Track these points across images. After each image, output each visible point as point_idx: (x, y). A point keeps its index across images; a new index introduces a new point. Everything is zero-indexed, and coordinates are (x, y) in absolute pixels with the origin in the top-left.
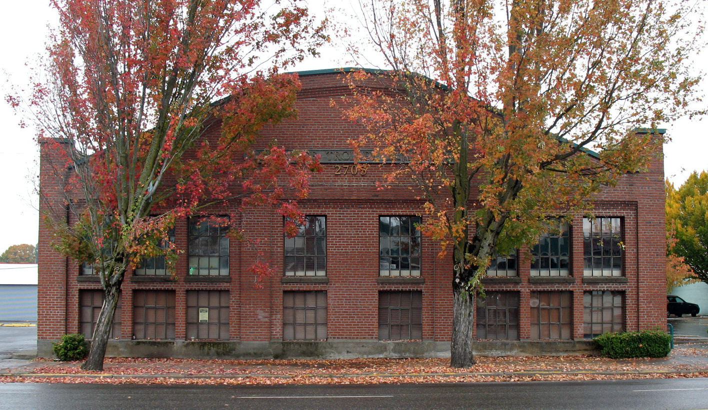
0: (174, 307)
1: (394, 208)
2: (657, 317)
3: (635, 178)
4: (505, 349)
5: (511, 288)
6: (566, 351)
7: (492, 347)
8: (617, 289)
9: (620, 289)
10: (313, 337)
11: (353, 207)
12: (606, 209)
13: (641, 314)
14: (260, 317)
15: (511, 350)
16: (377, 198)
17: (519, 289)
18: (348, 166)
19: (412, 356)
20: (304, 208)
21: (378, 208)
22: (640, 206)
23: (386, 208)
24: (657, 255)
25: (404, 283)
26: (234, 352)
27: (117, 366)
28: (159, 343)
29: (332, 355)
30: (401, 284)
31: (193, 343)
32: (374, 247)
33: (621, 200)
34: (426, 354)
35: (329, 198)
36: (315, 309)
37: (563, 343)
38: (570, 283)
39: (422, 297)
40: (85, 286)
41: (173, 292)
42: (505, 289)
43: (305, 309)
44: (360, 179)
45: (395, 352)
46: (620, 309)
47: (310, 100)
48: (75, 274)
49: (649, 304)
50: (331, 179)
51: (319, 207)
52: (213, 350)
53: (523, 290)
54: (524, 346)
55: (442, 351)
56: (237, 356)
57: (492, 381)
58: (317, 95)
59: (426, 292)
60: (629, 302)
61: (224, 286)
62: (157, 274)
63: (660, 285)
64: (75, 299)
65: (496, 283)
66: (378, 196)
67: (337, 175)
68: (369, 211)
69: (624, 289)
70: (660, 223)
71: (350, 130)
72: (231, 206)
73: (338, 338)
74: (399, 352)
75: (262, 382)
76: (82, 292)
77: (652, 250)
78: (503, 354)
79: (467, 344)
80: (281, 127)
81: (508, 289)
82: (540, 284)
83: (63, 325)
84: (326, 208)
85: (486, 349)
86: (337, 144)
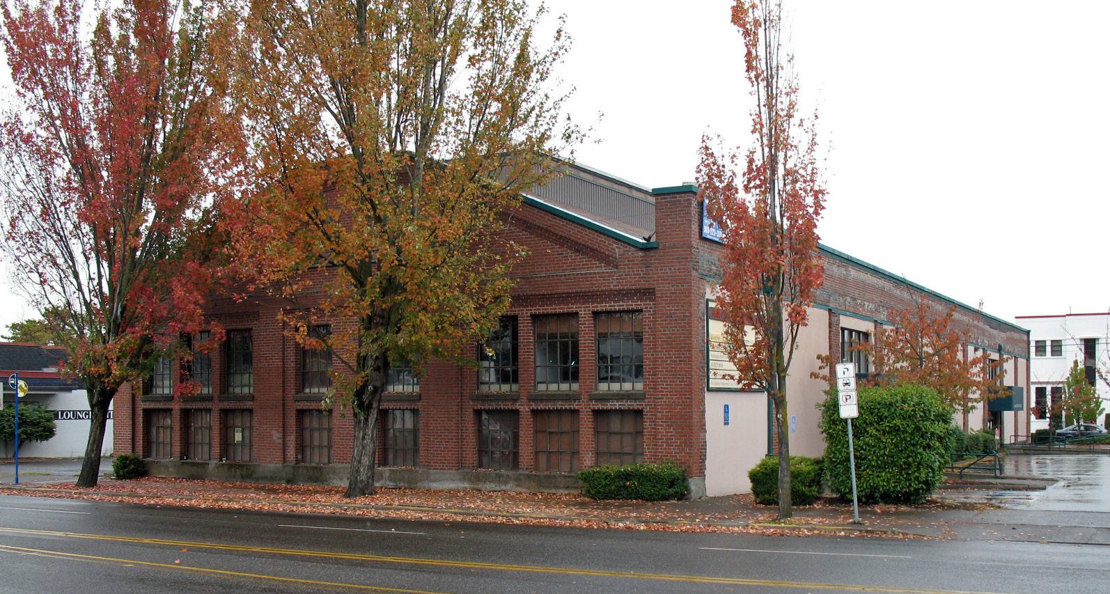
0: (578, 431)
2: (680, 446)
3: (653, 256)
4: (500, 482)
5: (510, 406)
6: (568, 487)
7: (486, 478)
8: (631, 408)
9: (636, 408)
10: (248, 458)
12: (619, 301)
14: (275, 438)
15: (506, 483)
17: (518, 407)
19: (406, 485)
24: (680, 361)
25: (402, 401)
26: (254, 476)
28: (198, 463)
29: (334, 481)
30: (399, 401)
31: (223, 464)
33: (634, 287)
34: (420, 484)
37: (564, 476)
38: (575, 400)
39: (643, 418)
40: (226, 405)
41: (575, 412)
42: (502, 407)
45: (390, 481)
48: (291, 391)
49: (670, 429)
52: (239, 472)
53: (522, 409)
54: (521, 480)
55: (434, 481)
56: (257, 480)
57: (331, 513)
61: (248, 405)
62: (572, 389)
63: (683, 402)
64: (140, 419)
65: (491, 401)
69: (640, 407)
70: (676, 320)
73: (343, 463)
74: (395, 481)
75: (266, 508)
76: (148, 413)
77: (674, 354)
78: (498, 488)
79: (360, 472)
81: (506, 408)
82: (541, 400)
85: (479, 481)
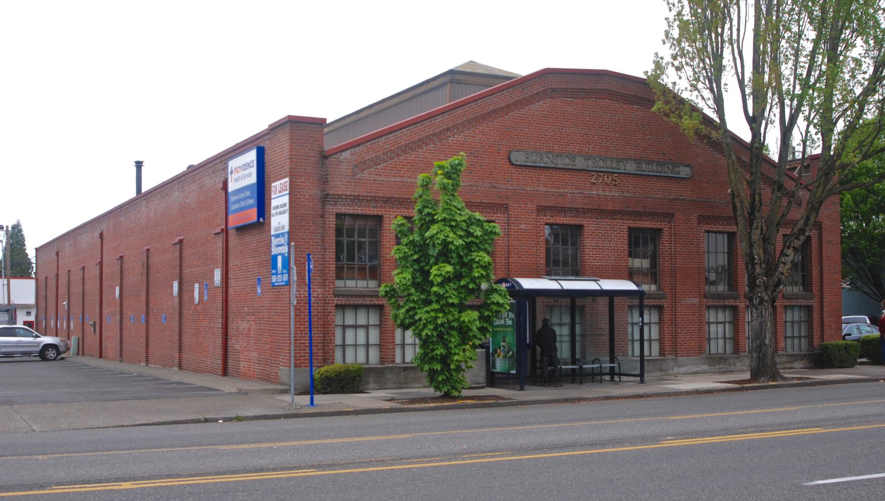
1: (640, 220)
11: (607, 217)
13: (825, 328)
16: (629, 209)
17: (738, 304)
18: (602, 174)
20: (565, 216)
21: (628, 220)
22: (823, 226)
23: (635, 220)
27: (505, 437)
32: (588, 265)
35: (589, 207)
36: (367, 327)
43: (356, 327)
44: (612, 188)
46: (355, 324)
47: (567, 101)
50: (587, 187)
51: (577, 217)
58: (575, 96)
59: (667, 307)
60: (816, 317)
66: (629, 207)
67: (593, 183)
68: (620, 223)
71: (603, 136)
72: (497, 212)
80: (543, 127)
83: (307, 360)
84: (584, 217)
86: (592, 150)
